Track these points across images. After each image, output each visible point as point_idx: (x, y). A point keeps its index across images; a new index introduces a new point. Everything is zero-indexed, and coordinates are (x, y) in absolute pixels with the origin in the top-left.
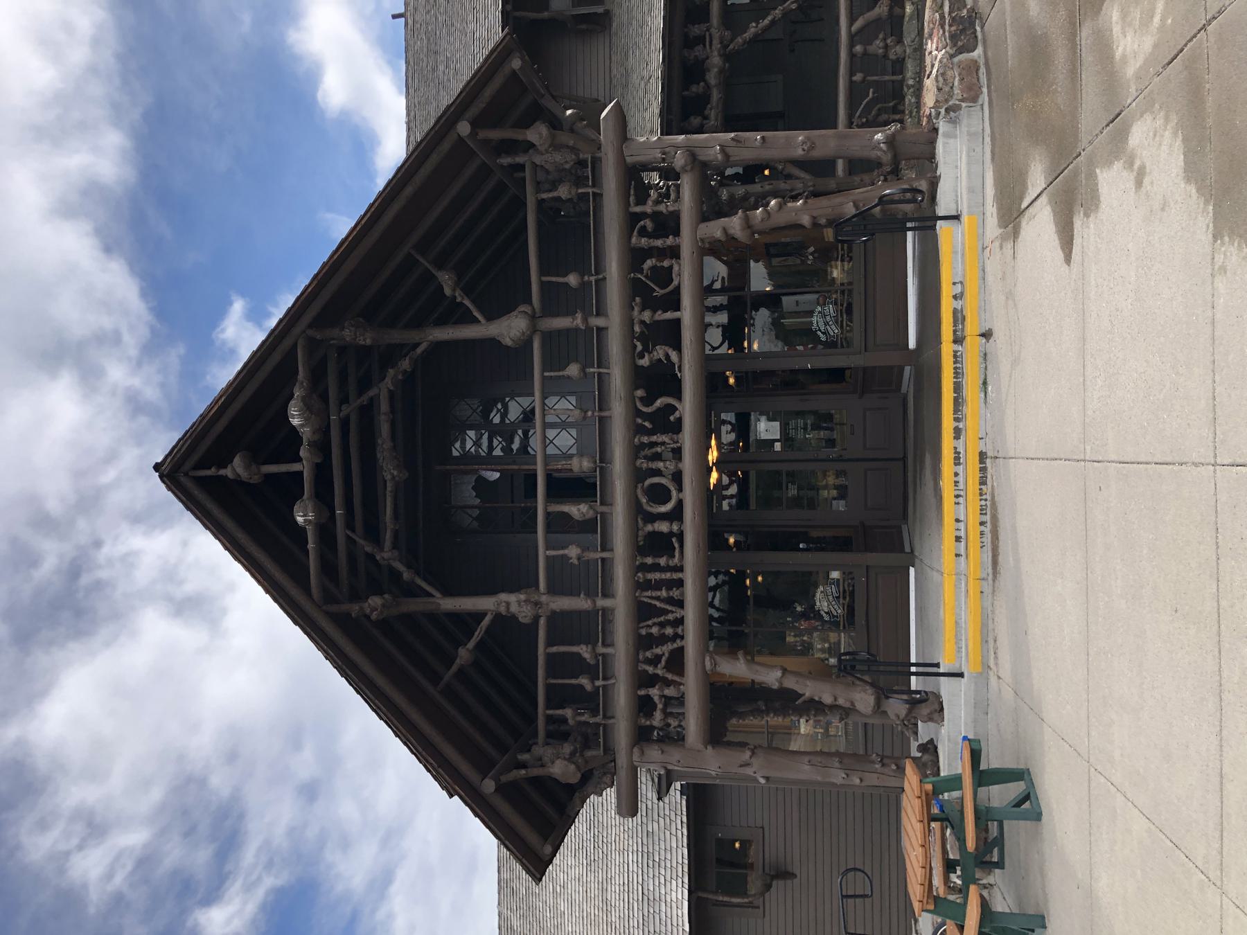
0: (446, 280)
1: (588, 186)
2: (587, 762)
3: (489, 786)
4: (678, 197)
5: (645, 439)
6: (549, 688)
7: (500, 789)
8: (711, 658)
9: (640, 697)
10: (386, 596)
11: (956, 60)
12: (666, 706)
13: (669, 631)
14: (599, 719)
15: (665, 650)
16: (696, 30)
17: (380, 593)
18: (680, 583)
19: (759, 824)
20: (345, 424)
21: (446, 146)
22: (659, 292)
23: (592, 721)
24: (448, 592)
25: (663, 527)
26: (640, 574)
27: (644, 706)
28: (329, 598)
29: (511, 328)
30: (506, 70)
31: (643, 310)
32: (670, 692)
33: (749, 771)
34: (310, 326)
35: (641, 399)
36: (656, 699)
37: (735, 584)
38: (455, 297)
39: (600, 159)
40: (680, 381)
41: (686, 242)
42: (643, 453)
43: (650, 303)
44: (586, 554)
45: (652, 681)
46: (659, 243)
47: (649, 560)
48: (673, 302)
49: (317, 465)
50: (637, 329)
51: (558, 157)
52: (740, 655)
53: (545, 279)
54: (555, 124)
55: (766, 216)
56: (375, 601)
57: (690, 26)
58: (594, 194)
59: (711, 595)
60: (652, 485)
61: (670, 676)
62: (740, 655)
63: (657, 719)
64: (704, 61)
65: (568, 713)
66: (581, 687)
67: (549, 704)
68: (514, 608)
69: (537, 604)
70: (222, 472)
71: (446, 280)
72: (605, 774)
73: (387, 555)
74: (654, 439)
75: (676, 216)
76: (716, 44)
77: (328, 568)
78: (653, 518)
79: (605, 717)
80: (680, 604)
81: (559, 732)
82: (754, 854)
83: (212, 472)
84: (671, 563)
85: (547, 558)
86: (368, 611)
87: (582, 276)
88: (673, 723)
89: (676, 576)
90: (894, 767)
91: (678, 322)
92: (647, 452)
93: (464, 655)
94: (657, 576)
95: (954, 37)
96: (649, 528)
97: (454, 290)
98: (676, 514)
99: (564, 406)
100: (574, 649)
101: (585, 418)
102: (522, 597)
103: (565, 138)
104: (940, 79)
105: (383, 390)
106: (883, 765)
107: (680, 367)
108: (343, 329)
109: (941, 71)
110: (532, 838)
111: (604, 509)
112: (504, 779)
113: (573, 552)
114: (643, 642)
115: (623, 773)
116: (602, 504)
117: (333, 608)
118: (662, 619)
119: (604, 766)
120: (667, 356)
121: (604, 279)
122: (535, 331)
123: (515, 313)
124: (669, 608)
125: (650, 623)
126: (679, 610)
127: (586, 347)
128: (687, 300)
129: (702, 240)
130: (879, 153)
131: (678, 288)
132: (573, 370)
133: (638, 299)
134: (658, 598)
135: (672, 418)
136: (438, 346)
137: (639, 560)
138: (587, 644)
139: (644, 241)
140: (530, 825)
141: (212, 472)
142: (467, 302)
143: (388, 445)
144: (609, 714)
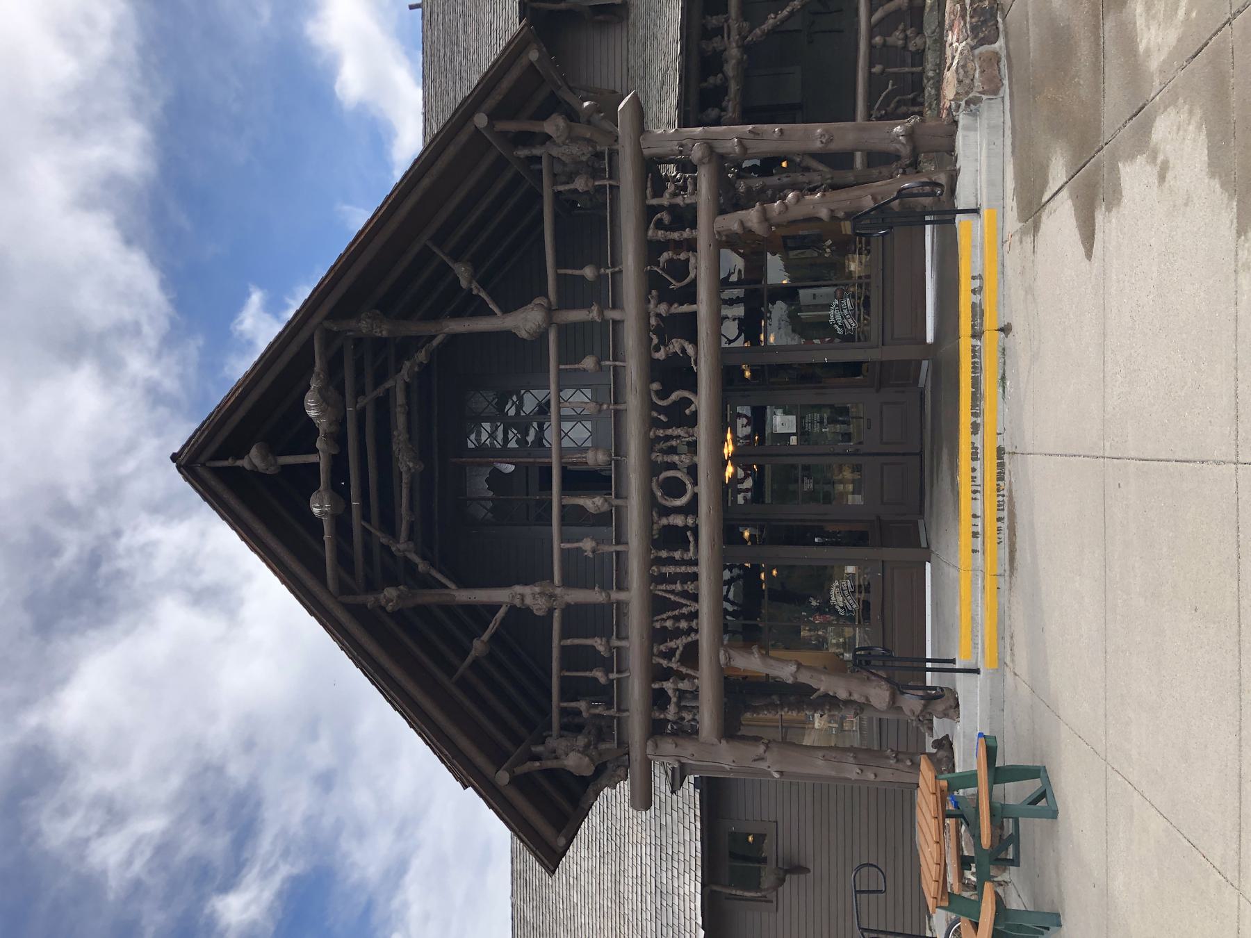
0: (462, 272)
1: (604, 178)
2: (600, 755)
3: (503, 777)
5: (661, 433)
7: (515, 781)
10: (401, 587)
13: (683, 625)
14: (613, 712)
15: (680, 643)
16: (714, 21)
18: (695, 577)
21: (463, 137)
22: (675, 285)
23: (606, 713)
25: (678, 521)
27: (658, 699)
28: (344, 589)
29: (526, 321)
30: (523, 62)
33: (763, 765)
34: (327, 318)
35: (657, 392)
36: (670, 693)
42: (658, 447)
43: (668, 296)
45: (666, 674)
46: (675, 235)
47: (664, 554)
48: (690, 294)
49: (333, 456)
50: (653, 321)
51: (575, 149)
52: (755, 649)
54: (572, 116)
56: (390, 592)
58: (611, 186)
62: (755, 649)
65: (582, 705)
66: (596, 679)
67: (564, 696)
68: (529, 601)
69: (552, 596)
70: (239, 463)
71: (462, 272)
73: (401, 546)
74: (669, 432)
75: (693, 209)
76: (735, 36)
77: (344, 559)
78: (667, 511)
79: (619, 710)
80: (695, 598)
81: (572, 725)
82: (768, 849)
83: (228, 463)
86: (383, 602)
88: (687, 716)
89: (691, 569)
91: (694, 315)
92: (663, 445)
93: (479, 647)
95: (975, 29)
96: (664, 521)
97: (470, 283)
98: (692, 508)
99: (580, 398)
100: (589, 642)
101: (600, 411)
102: (537, 589)
104: (961, 71)
105: (398, 383)
112: (519, 770)
113: (587, 545)
114: (657, 636)
115: (636, 766)
117: (350, 599)
118: (676, 612)
120: (683, 350)
121: (621, 271)
123: (530, 306)
125: (664, 616)
126: (693, 604)
127: (604, 339)
129: (719, 233)
130: (898, 146)
131: (694, 283)
132: (589, 363)
134: (672, 592)
135: (687, 412)
136: (454, 338)
137: (654, 554)
138: (601, 637)
139: (661, 234)
140: (544, 817)
141: (228, 463)
142: (483, 295)
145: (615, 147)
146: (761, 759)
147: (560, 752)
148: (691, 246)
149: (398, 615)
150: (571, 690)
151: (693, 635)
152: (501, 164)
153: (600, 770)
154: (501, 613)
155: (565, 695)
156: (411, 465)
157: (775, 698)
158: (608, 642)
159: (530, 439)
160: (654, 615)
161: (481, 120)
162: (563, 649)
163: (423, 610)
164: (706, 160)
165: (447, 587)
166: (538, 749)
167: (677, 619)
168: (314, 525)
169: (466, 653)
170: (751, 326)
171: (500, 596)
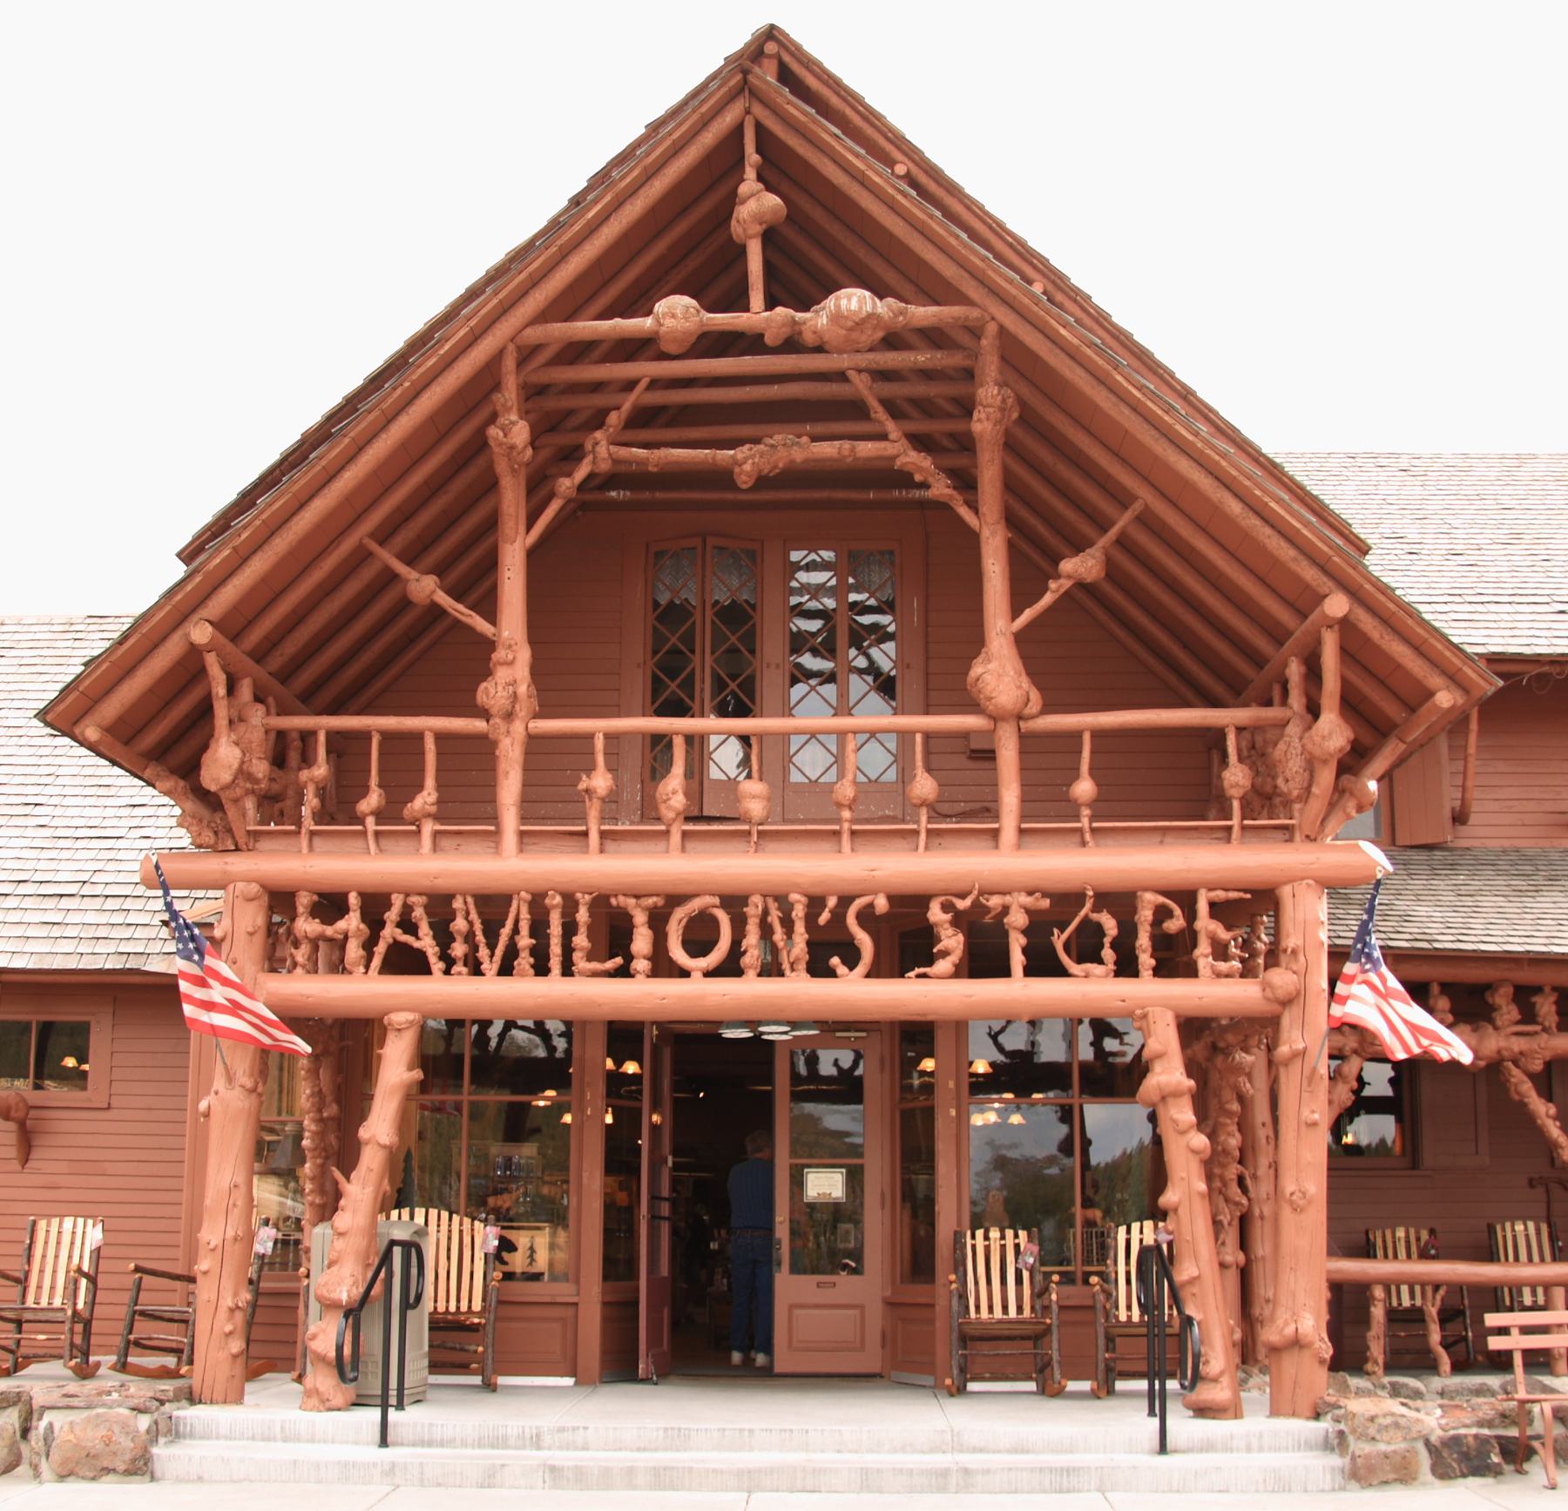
0: (1082, 566)
1: (1243, 818)
2: (236, 801)
3: (201, 633)
4: (1219, 975)
5: (799, 912)
6: (364, 736)
7: (194, 653)
8: (411, 1023)
9: (345, 896)
10: (529, 452)
11: (1420, 1446)
12: (330, 940)
13: (459, 949)
14: (309, 824)
15: (426, 942)
16: (1546, 1007)
17: (533, 443)
18: (541, 969)
19: (114, 1103)
20: (841, 376)
21: (1310, 574)
22: (1059, 940)
23: (305, 811)
24: (533, 555)
25: (642, 942)
26: (558, 899)
27: (330, 905)
28: (527, 354)
29: (1000, 674)
30: (1434, 680)
31: (1028, 911)
32: (354, 951)
33: (219, 1083)
34: (1002, 330)
35: (871, 905)
36: (341, 925)
37: (555, 1072)
38: (1057, 576)
39: (1290, 840)
40: (902, 975)
41: (1147, 989)
42: (773, 906)
43: (1038, 928)
44: (596, 804)
45: (374, 923)
46: (1144, 940)
47: (583, 916)
48: (1043, 964)
49: (762, 336)
50: (995, 901)
51: (1295, 765)
52: (418, 1074)
53: (1087, 737)
54: (1352, 762)
55: (1182, 1127)
56: (520, 433)
57: (1552, 998)
58: (1229, 829)
59: (530, 1024)
60: (715, 922)
61: (380, 949)
62: (418, 1074)
63: (307, 926)
64: (1491, 1021)
65: (321, 770)
66: (364, 791)
67: (334, 737)
68: (502, 674)
69: (509, 716)
70: (750, 174)
71: (1082, 566)
72: (216, 833)
73: (602, 451)
74: (800, 928)
75: (1191, 971)
76: (1517, 1044)
77: (578, 351)
78: (658, 922)
79: (312, 834)
80: (506, 970)
81: (285, 752)
82: (54, 1092)
83: (752, 157)
84: (577, 956)
85: (589, 737)
86: (501, 420)
87: (1090, 805)
88: (301, 955)
89: (555, 963)
90: (229, 1328)
91: (1005, 972)
92: (774, 917)
93: (424, 587)
94: (555, 930)
95: (1455, 1442)
96: (640, 918)
97: (1069, 577)
98: (663, 967)
99: (876, 761)
100: (430, 782)
101: (839, 805)
102: (523, 689)
103: (1326, 776)
104: (1389, 1420)
105: (896, 449)
106: (232, 1310)
107: (924, 976)
108: (1002, 384)
109: (1402, 1421)
110: (112, 707)
111: (676, 837)
112: (212, 661)
113: (600, 781)
114: (440, 905)
115: (214, 865)
116: (685, 834)
117: (509, 363)
118: (480, 938)
119: (230, 831)
120: (945, 954)
121: (1084, 844)
122: (995, 719)
123: (1025, 683)
124: (499, 951)
125: (474, 916)
126: (496, 967)
127: (968, 812)
128: (1046, 990)
129: (1145, 1016)
130: (1280, 1322)
131: (1062, 972)
132: (924, 786)
133: (1046, 903)
134: (516, 930)
135: (835, 961)
136: (972, 541)
137: (584, 899)
138: (439, 802)
139: (1145, 915)
140: (143, 711)
141: (752, 157)
142: (1047, 599)
143: (798, 455)
144: (317, 841)
145: (1298, 837)
146: (230, 1079)
147: (242, 728)
148: (1126, 967)
149: (479, 445)
150: (345, 747)
151: (441, 965)
152: (1278, 636)
153: (210, 801)
154: (480, 624)
155: (341, 744)
156: (747, 467)
157: (331, 1110)
158: (429, 815)
159: (809, 661)
160: (474, 896)
161: (1337, 605)
162: (417, 737)
163: (491, 485)
164: (1269, 993)
165: (529, 528)
166: (246, 690)
167: (469, 937)
168: (638, 301)
169: (411, 557)
170: (1019, 1074)
171: (511, 625)
